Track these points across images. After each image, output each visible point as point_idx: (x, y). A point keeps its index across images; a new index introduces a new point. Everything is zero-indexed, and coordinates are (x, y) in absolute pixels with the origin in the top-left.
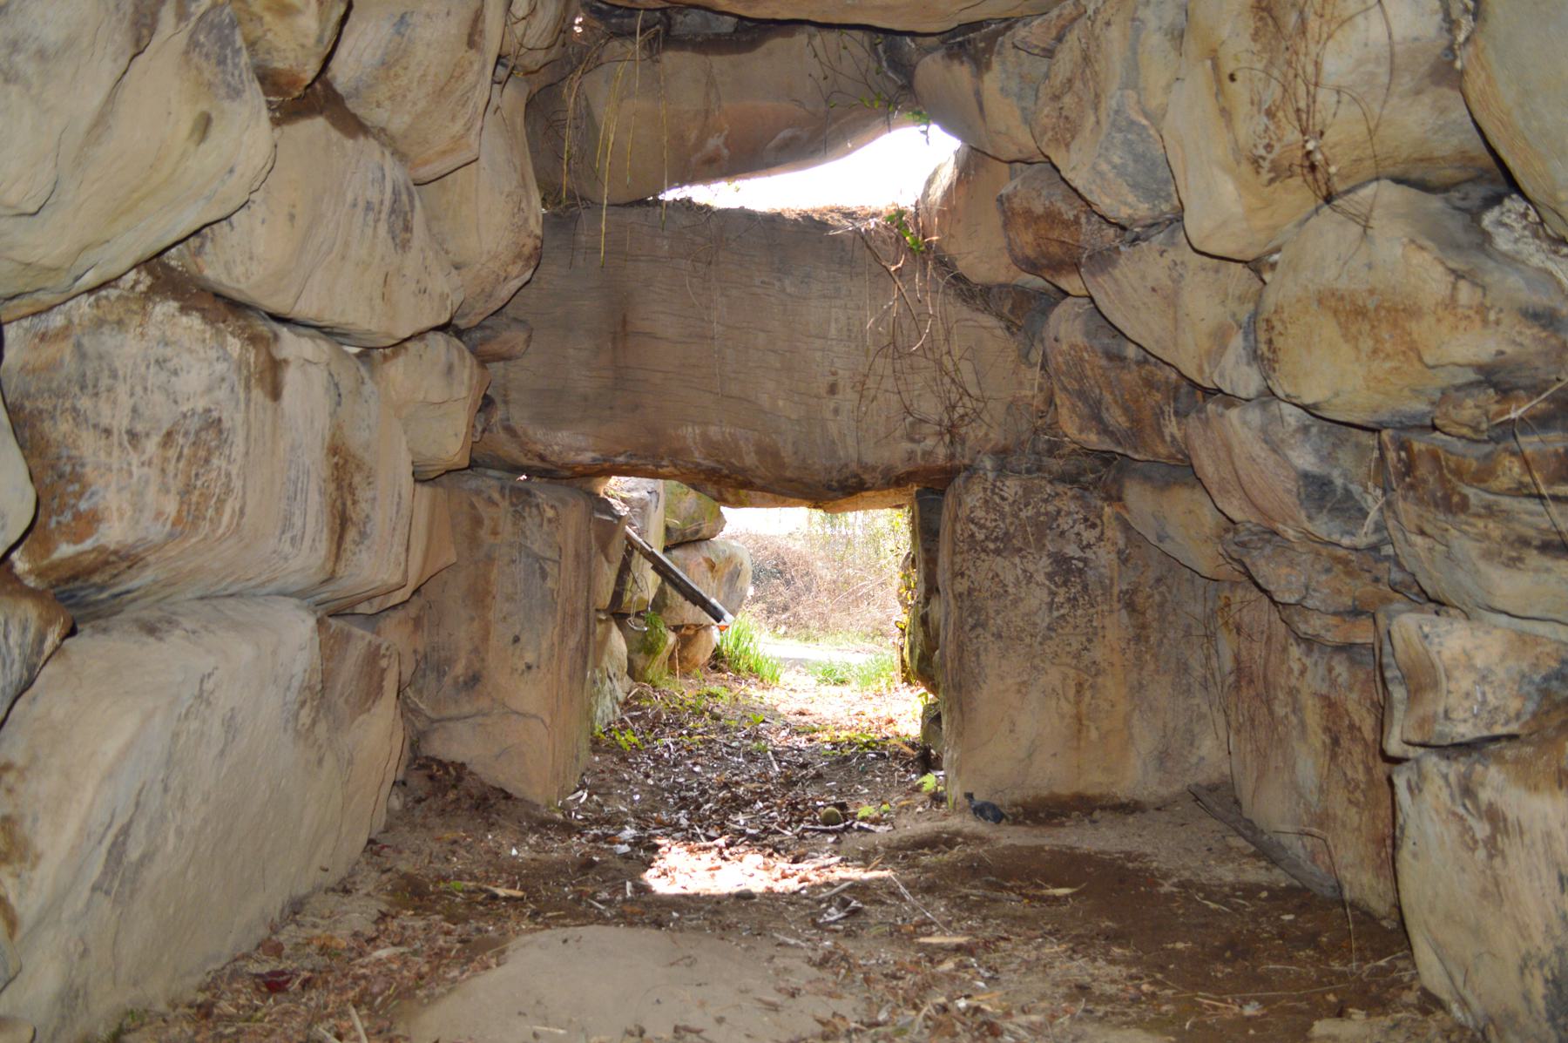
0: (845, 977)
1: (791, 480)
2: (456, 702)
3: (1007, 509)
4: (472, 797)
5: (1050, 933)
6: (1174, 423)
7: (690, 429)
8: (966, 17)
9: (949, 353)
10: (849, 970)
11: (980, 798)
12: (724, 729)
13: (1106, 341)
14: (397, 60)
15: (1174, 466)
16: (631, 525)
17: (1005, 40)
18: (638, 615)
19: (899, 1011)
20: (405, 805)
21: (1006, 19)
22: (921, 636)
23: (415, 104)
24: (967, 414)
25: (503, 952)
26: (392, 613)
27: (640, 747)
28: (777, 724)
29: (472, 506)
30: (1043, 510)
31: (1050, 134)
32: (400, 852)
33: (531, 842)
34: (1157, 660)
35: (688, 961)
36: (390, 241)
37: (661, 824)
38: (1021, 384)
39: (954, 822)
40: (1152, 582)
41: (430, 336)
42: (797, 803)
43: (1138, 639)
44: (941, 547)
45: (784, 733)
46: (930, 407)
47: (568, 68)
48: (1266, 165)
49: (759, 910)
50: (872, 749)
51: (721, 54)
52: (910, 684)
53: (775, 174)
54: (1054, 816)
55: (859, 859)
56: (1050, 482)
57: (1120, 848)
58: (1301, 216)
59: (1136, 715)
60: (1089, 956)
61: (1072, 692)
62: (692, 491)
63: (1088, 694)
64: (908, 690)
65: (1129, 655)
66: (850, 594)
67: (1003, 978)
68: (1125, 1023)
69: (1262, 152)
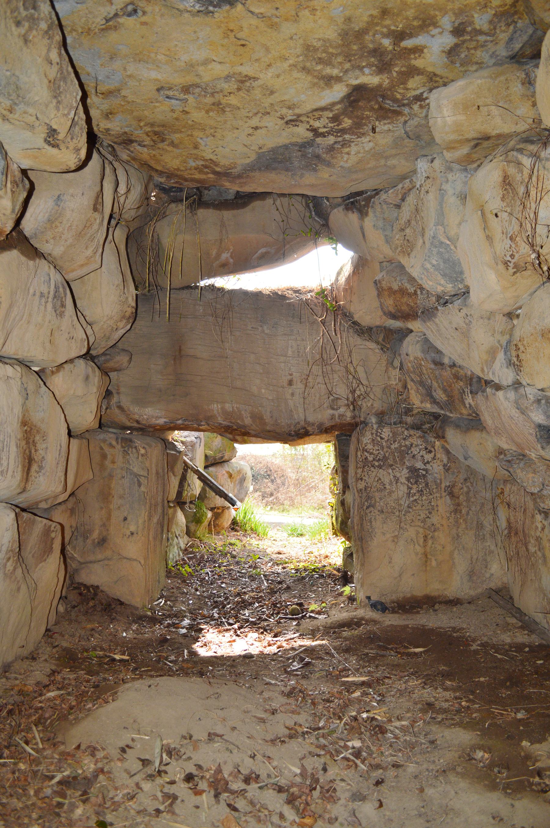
0: (301, 702)
1: (269, 431)
2: (94, 553)
3: (384, 444)
4: (102, 605)
5: (412, 674)
6: (470, 397)
7: (215, 406)
8: (354, 190)
9: (351, 362)
10: (304, 698)
11: (374, 598)
12: (238, 563)
13: (433, 355)
14: (56, 219)
15: (472, 420)
16: (186, 455)
17: (375, 200)
18: (191, 502)
19: (331, 720)
20: (66, 609)
21: (375, 190)
22: (341, 511)
23: (66, 241)
24: (362, 394)
25: (116, 693)
26: (58, 507)
27: (193, 574)
28: (267, 559)
29: (101, 448)
30: (403, 444)
31: (400, 249)
32: (63, 636)
33: (134, 628)
34: (466, 523)
35: (216, 696)
36: (54, 312)
37: (204, 617)
38: (389, 378)
39: (361, 613)
40: (462, 481)
41: (77, 361)
42: (277, 604)
43: (456, 511)
44: (350, 463)
45: (270, 564)
46: (342, 391)
47: (148, 219)
48: (511, 265)
49: (255, 664)
50: (317, 572)
51: (228, 210)
52: (337, 535)
53: (258, 271)
54: (414, 607)
55: (310, 634)
56: (407, 429)
57: (449, 625)
58: (532, 290)
59: (456, 551)
60: (433, 686)
61: (422, 540)
62: (219, 436)
63: (430, 542)
64: (336, 539)
65: (452, 520)
66: (306, 486)
67: (387, 700)
68: (453, 725)
69: (509, 258)
